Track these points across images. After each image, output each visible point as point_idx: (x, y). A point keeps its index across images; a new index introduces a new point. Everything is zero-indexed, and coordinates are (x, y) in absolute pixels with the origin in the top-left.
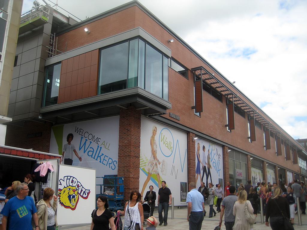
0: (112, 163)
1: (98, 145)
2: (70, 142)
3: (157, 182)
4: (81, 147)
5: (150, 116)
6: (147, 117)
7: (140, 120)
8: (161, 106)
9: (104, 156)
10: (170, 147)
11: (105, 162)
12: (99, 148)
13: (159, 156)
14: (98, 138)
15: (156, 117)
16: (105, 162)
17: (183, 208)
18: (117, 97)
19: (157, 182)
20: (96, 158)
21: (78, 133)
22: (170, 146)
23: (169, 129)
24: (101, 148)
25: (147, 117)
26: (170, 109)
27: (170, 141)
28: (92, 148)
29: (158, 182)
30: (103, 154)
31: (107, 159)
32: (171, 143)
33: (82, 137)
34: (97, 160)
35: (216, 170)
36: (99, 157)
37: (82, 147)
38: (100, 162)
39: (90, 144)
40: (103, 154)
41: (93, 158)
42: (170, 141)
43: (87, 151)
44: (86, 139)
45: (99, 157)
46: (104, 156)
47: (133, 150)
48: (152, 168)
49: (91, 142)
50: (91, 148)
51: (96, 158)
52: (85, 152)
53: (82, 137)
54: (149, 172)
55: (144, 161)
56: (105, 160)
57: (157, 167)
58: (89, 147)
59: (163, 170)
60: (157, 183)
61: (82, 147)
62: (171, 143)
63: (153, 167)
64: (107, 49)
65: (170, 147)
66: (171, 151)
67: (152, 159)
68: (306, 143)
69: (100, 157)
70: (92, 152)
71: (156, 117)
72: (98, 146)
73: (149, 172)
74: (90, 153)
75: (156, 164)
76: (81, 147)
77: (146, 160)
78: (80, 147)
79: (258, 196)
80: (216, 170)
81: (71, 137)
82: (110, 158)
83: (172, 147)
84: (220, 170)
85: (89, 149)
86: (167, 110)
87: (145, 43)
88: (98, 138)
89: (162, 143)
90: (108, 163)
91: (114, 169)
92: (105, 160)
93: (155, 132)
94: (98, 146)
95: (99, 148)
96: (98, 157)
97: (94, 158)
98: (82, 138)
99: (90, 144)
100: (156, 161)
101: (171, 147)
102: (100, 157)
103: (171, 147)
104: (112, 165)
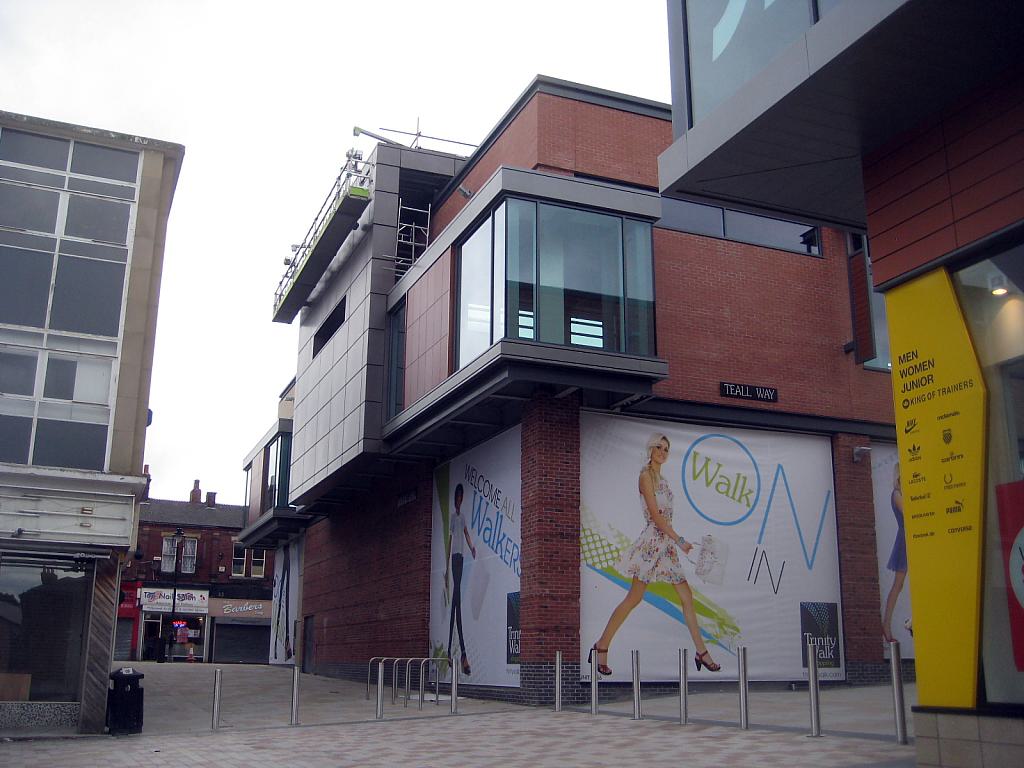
3: (680, 608)
4: (780, 471)
5: (623, 408)
6: (618, 410)
7: (577, 426)
13: (683, 523)
19: (680, 608)
20: (737, 496)
23: (741, 439)
25: (618, 410)
26: (663, 379)
29: (683, 604)
32: (745, 478)
34: (739, 501)
47: (548, 517)
48: (653, 564)
49: (488, 504)
50: (721, 476)
51: (737, 496)
52: (708, 484)
54: (635, 578)
55: (609, 545)
57: (673, 561)
59: (706, 567)
60: (677, 610)
62: (502, 516)
63: (654, 561)
66: (748, 505)
67: (651, 534)
69: (746, 495)
73: (635, 578)
75: (670, 552)
76: (780, 471)
77: (621, 542)
78: (707, 480)
85: (717, 480)
86: (654, 386)
89: (696, 487)
97: (733, 498)
98: (476, 493)
100: (672, 542)
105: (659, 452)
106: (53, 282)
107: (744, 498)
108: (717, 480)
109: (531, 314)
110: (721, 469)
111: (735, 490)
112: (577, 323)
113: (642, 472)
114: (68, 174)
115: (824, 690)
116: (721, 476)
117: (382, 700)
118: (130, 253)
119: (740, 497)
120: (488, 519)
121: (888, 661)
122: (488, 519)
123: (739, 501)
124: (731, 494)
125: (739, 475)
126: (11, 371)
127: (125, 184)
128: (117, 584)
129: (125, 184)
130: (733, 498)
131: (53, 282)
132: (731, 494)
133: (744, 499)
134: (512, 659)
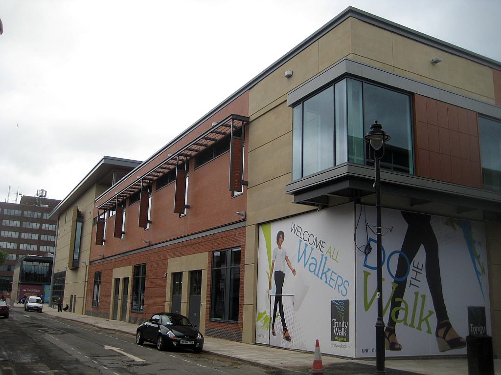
0: (341, 285)
1: (323, 253)
2: (280, 245)
4: (300, 256)
9: (331, 271)
11: (333, 283)
14: (321, 241)
16: (333, 283)
18: (302, 188)
20: (416, 324)
21: (296, 233)
24: (326, 258)
28: (315, 259)
30: (329, 270)
31: (334, 277)
33: (300, 240)
34: (419, 328)
36: (425, 321)
37: (301, 257)
38: (326, 282)
39: (311, 252)
40: (329, 270)
41: (417, 328)
43: (308, 265)
44: (311, 248)
45: (425, 321)
46: (331, 271)
49: (312, 249)
50: (312, 258)
51: (416, 324)
53: (300, 240)
56: (333, 279)
58: (311, 257)
61: (301, 257)
64: (320, 94)
68: (4, 210)
69: (426, 319)
70: (314, 266)
72: (323, 255)
74: (313, 267)
81: (281, 236)
82: (339, 276)
87: (362, 82)
88: (321, 241)
90: (337, 286)
91: (346, 295)
92: (333, 279)
94: (323, 255)
95: (324, 259)
96: (421, 320)
97: (412, 325)
98: (301, 241)
99: (311, 252)
102: (426, 319)
104: (342, 288)
107: (424, 323)
108: (311, 261)
109: (381, 180)
111: (320, 266)
113: (400, 345)
116: (312, 258)
119: (420, 325)
121: (220, 267)
123: (419, 328)
126: (3, 313)
127: (111, 315)
129: (111, 315)
130: (317, 275)
133: (424, 324)
134: (133, 311)
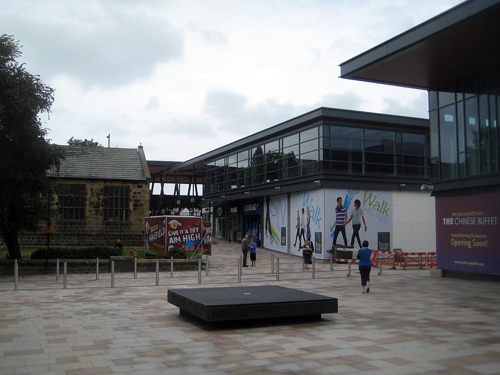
8: (192, 219)
10: (383, 209)
12: (385, 204)
15: (426, 321)
17: (371, 325)
20: (382, 212)
22: (384, 207)
27: (318, 207)
35: (314, 221)
42: (318, 207)
43: (373, 205)
51: (382, 212)
65: (383, 209)
71: (426, 321)
78: (370, 202)
79: (9, 256)
80: (314, 221)
83: (321, 219)
84: (321, 219)
85: (374, 203)
93: (308, 237)
101: (319, 219)
103: (319, 219)
105: (371, 194)
106: (339, 161)
108: (374, 203)
110: (376, 199)
112: (23, 248)
114: (403, 154)
115: (28, 278)
116: (376, 202)
117: (170, 215)
118: (212, 223)
120: (312, 207)
122: (312, 207)
124: (379, 210)
125: (384, 201)
128: (137, 203)
131: (339, 161)
132: (379, 210)
